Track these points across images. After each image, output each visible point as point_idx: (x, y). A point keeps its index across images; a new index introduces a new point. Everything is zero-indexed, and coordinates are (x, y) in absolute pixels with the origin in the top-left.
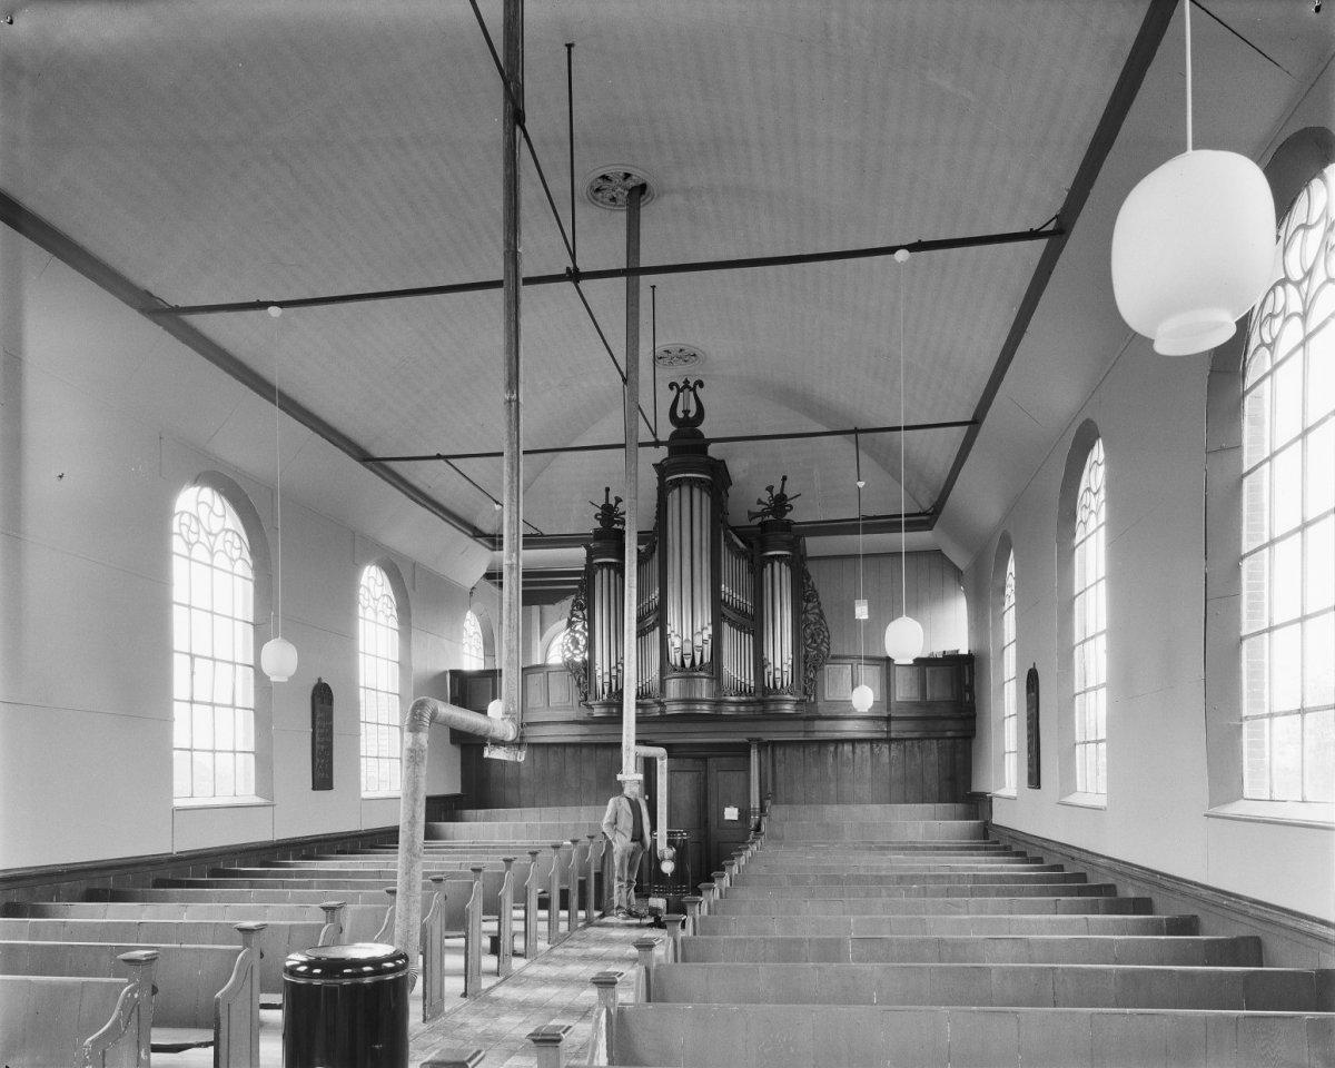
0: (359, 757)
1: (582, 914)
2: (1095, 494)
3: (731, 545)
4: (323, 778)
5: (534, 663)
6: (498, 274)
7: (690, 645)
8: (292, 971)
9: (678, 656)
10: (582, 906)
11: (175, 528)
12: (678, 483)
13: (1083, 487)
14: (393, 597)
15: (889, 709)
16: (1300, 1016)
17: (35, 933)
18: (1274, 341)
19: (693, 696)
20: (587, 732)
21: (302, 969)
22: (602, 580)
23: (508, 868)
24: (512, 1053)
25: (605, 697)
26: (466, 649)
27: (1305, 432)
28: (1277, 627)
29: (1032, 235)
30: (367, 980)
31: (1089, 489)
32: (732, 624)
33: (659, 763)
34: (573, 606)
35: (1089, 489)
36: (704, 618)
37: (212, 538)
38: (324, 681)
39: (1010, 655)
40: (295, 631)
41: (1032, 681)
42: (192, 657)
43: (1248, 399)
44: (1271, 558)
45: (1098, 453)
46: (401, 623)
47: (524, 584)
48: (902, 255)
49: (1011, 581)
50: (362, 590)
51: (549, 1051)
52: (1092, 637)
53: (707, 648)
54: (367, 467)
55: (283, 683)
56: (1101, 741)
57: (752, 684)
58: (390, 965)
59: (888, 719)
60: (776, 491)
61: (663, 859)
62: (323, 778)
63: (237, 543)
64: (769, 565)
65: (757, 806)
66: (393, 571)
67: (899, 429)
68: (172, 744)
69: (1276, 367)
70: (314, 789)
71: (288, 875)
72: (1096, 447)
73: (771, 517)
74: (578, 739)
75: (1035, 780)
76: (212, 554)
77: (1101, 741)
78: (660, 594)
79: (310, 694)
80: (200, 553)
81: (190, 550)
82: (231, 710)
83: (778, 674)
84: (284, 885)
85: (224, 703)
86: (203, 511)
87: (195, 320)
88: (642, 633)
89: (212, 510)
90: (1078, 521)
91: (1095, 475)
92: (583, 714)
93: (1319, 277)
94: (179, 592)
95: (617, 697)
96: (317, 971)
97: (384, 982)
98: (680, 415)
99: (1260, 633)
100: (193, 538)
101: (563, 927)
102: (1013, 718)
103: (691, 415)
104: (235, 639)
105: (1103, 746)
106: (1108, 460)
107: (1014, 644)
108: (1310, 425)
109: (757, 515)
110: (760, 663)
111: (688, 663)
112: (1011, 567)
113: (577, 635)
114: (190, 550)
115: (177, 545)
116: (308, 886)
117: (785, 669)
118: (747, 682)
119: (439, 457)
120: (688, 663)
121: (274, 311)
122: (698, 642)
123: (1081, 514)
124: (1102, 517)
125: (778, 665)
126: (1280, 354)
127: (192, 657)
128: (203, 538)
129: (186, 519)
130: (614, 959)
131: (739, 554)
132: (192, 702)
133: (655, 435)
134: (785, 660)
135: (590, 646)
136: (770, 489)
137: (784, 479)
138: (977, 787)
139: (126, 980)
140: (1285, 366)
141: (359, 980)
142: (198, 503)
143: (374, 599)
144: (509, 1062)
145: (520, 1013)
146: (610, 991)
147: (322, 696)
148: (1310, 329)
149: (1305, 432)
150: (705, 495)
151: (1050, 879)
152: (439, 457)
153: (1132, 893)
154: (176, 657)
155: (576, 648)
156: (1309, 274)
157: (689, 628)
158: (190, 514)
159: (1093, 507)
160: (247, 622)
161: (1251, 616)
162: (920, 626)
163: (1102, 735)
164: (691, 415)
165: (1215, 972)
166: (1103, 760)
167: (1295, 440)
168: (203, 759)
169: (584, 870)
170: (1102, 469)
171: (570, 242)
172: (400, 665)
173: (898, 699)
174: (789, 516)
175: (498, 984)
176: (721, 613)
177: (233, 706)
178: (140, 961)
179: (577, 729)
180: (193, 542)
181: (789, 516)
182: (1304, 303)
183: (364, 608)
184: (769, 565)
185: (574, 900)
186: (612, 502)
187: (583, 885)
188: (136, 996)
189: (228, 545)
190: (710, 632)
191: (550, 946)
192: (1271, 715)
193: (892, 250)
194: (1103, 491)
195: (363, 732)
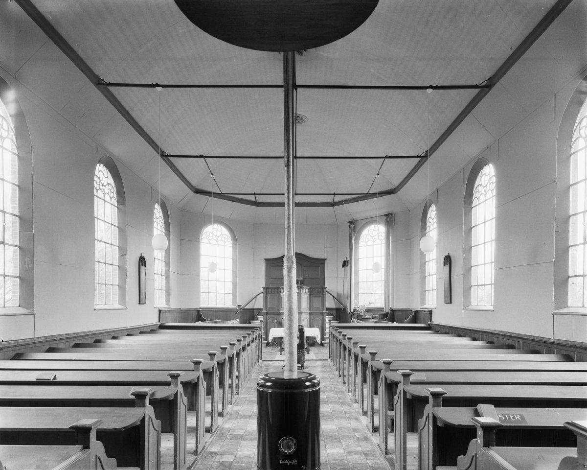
2: (484, 187)
17: (216, 368)
18: (479, 198)
31: (431, 217)
37: (104, 187)
38: (143, 255)
46: (166, 229)
50: (95, 178)
76: (104, 195)
89: (103, 175)
96: (269, 384)
123: (428, 224)
140: (488, 201)
143: (103, 185)
146: (407, 378)
148: (487, 199)
156: (486, 186)
159: (432, 223)
171: (427, 421)
182: (485, 192)
183: (96, 189)
189: (109, 191)
192: (478, 286)
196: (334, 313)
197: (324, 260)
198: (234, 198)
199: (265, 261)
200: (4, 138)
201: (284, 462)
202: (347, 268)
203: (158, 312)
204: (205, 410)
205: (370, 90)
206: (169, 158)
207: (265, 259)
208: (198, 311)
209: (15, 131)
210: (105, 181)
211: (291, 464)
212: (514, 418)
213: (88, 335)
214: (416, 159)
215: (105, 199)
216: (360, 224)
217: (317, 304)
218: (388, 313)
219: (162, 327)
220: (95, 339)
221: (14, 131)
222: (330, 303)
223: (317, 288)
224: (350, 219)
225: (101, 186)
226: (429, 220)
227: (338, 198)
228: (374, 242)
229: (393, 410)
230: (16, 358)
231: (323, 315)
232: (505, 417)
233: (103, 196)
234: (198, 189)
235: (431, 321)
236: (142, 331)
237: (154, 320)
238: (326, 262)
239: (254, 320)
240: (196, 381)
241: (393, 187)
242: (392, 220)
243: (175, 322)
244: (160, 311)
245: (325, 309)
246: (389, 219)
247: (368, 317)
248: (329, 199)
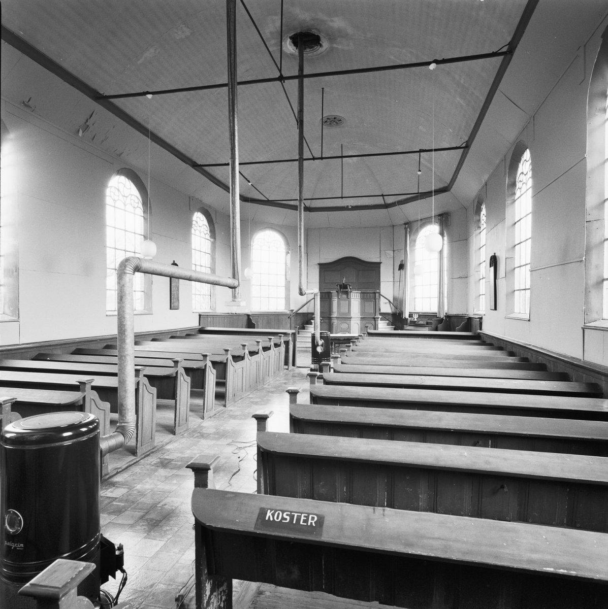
2: (525, 175)
6: (297, 157)
14: (208, 226)
35: (522, 173)
45: (527, 155)
48: (432, 66)
50: (194, 223)
54: (195, 169)
61: (318, 345)
63: (137, 201)
72: (525, 153)
76: (125, 205)
86: (198, 220)
87: (206, 168)
90: (517, 187)
91: (525, 166)
100: (116, 198)
121: (149, 96)
128: (121, 197)
133: (280, 71)
146: (335, 360)
158: (115, 188)
160: (141, 235)
171: (279, 66)
172: (144, 236)
193: (429, 63)
196: (390, 318)
197: (380, 263)
198: (281, 204)
199: (318, 266)
202: (403, 272)
203: (198, 316)
204: (155, 422)
206: (203, 167)
207: (319, 264)
208: (248, 316)
212: (306, 521)
213: (93, 341)
214: (458, 150)
216: (415, 226)
217: (370, 309)
218: (443, 319)
219: (202, 331)
220: (105, 344)
222: (386, 308)
223: (369, 293)
224: (405, 221)
226: (520, 178)
227: (390, 200)
228: (269, 247)
230: (39, 358)
231: (375, 321)
232: (292, 517)
234: (247, 198)
235: (481, 329)
236: (175, 335)
237: (194, 324)
238: (382, 265)
239: (308, 324)
240: (81, 403)
241: (446, 185)
242: (447, 219)
243: (223, 327)
244: (200, 315)
245: (378, 313)
246: (444, 219)
247: (421, 322)
248: (379, 201)
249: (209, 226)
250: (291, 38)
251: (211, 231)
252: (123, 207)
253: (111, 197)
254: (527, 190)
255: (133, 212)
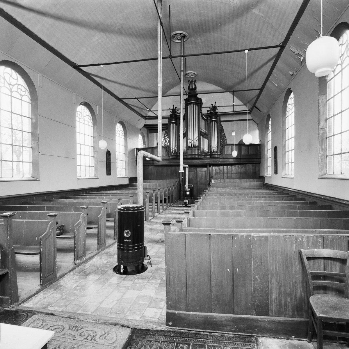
0: (116, 168)
1: (169, 204)
3: (203, 118)
4: (109, 173)
5: (155, 146)
7: (193, 142)
8: (120, 209)
9: (190, 144)
10: (169, 203)
11: (77, 115)
12: (191, 104)
13: (288, 104)
15: (240, 156)
16: (341, 219)
18: (334, 70)
19: (195, 154)
20: (169, 162)
21: (122, 209)
22: (173, 127)
23: (154, 192)
24: (158, 233)
25: (173, 154)
26: (139, 143)
27: (342, 91)
28: (335, 135)
29: (277, 46)
30: (136, 211)
32: (203, 137)
33: (187, 168)
34: (165, 133)
35: (289, 104)
36: (196, 135)
37: (84, 117)
39: (270, 143)
40: (106, 138)
41: (276, 149)
42: (80, 144)
43: (328, 83)
44: (334, 119)
45: (292, 95)
47: (163, 127)
49: (270, 126)
50: (116, 129)
51: (180, 224)
52: (291, 138)
53: (197, 142)
55: (103, 150)
56: (293, 163)
57: (208, 151)
58: (140, 208)
59: (240, 159)
60: (214, 105)
62: (109, 173)
63: (90, 118)
64: (212, 123)
65: (209, 179)
66: (122, 123)
67: (246, 90)
68: (76, 164)
69: (335, 76)
70: (107, 175)
71: (104, 194)
72: (291, 94)
73: (212, 111)
74: (165, 164)
75: (276, 173)
76: (84, 121)
77: (293, 163)
78: (186, 130)
79: (106, 153)
80: (82, 121)
81: (80, 120)
82: (88, 157)
83: (214, 148)
84: (103, 196)
85: (87, 155)
86: (82, 111)
88: (184, 138)
91: (291, 100)
92: (167, 158)
93: (345, 55)
94: (78, 130)
95: (177, 155)
96: (126, 209)
97: (135, 212)
98: (191, 88)
99: (331, 136)
101: (165, 207)
102: (271, 158)
103: (193, 88)
104: (90, 141)
105: (293, 164)
106: (295, 98)
107: (271, 141)
108: (343, 89)
109: (209, 111)
110: (210, 146)
111: (193, 146)
112: (270, 122)
113: (166, 139)
114: (80, 120)
115: (77, 119)
116: (109, 196)
117: (216, 147)
118: (207, 150)
119: (135, 98)
120: (193, 146)
121: (102, 66)
122: (195, 141)
123: (288, 110)
124: (293, 110)
125: (214, 146)
126: (336, 73)
127: (80, 144)
128: (82, 117)
129: (79, 113)
130: (177, 214)
131: (205, 120)
132: (80, 155)
134: (216, 145)
135: (169, 142)
136: (212, 105)
137: (216, 102)
138: (261, 175)
139: (81, 212)
141: (134, 211)
142: (81, 109)
144: (158, 234)
145: (150, 231)
147: (108, 153)
148: (343, 68)
149: (342, 91)
150: (196, 106)
151: (280, 194)
152: (135, 98)
153: (300, 197)
154: (77, 144)
155: (166, 142)
157: (193, 137)
159: (291, 108)
161: (329, 132)
162: (251, 136)
163: (293, 161)
164: (193, 88)
165: (322, 211)
166: (293, 168)
167: (340, 92)
168: (83, 168)
169: (169, 194)
170: (293, 99)
173: (242, 154)
174: (217, 111)
175: (152, 219)
176: (201, 134)
177: (89, 156)
178: (84, 208)
179: (167, 161)
180: (80, 118)
181: (217, 111)
182: (342, 61)
184: (212, 123)
185: (167, 201)
186: (174, 108)
187: (169, 197)
188: (84, 215)
189: (88, 119)
190: (198, 138)
191: (162, 211)
192: (334, 155)
194: (293, 105)
195: (117, 162)
200: (23, 96)
201: (126, 240)
205: (347, 200)
209: (29, 91)
210: (85, 114)
211: (128, 241)
215: (80, 121)
221: (29, 91)
225: (82, 116)
226: (288, 106)
229: (161, 203)
233: (83, 121)
249: (124, 130)
250: (323, 329)
251: (124, 134)
252: (83, 122)
253: (18, 92)
254: (292, 113)
255: (10, 94)
